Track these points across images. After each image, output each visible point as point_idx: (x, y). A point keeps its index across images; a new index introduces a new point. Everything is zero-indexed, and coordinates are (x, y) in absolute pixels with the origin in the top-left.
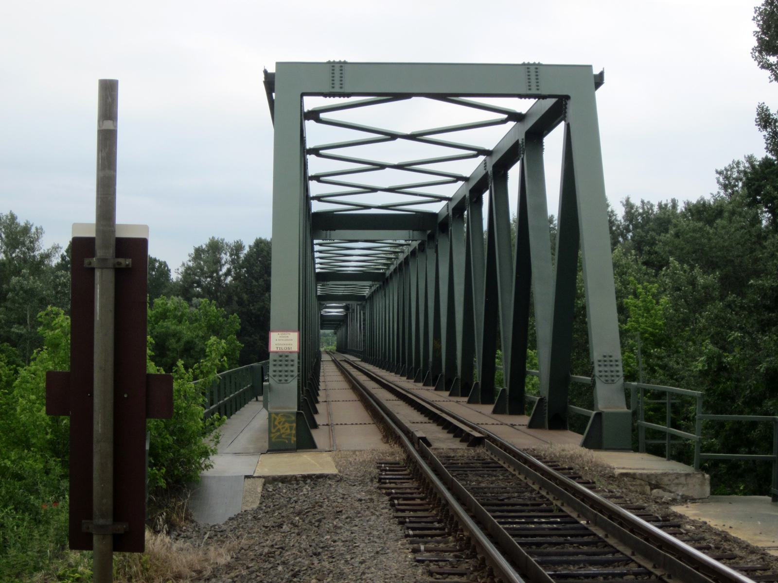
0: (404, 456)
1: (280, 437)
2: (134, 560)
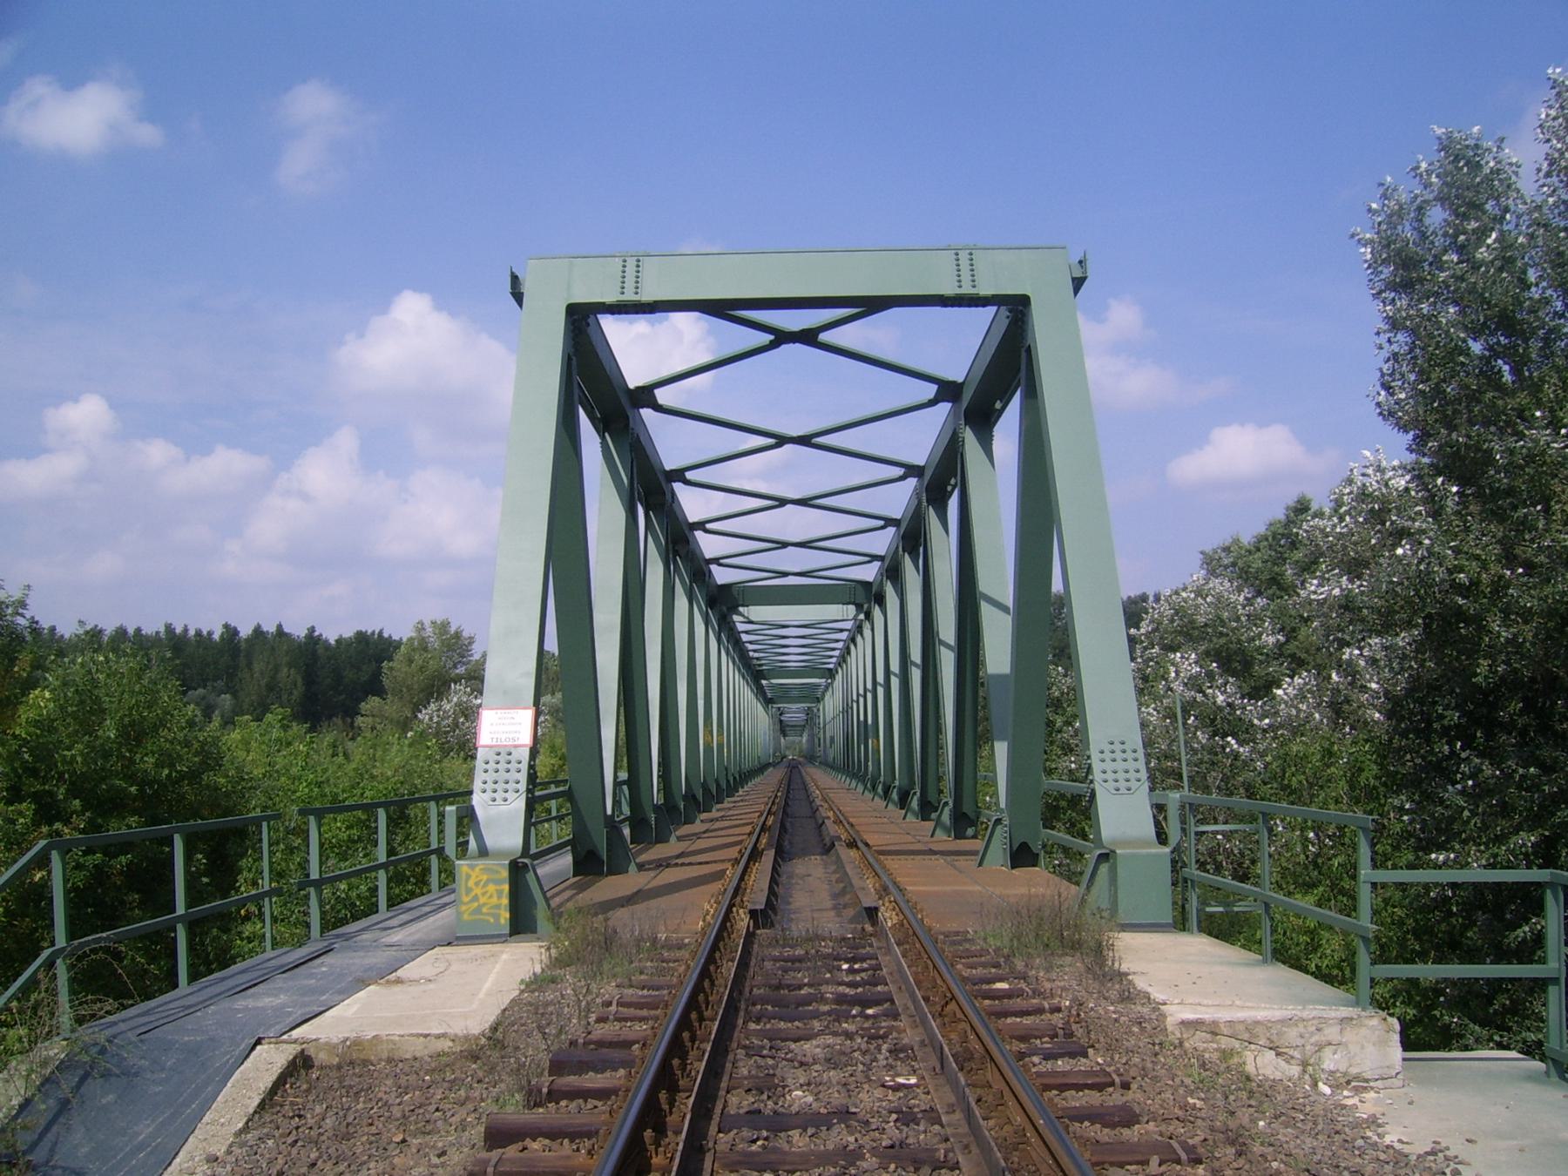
0: (799, 867)
1: (478, 911)
2: (885, 889)
